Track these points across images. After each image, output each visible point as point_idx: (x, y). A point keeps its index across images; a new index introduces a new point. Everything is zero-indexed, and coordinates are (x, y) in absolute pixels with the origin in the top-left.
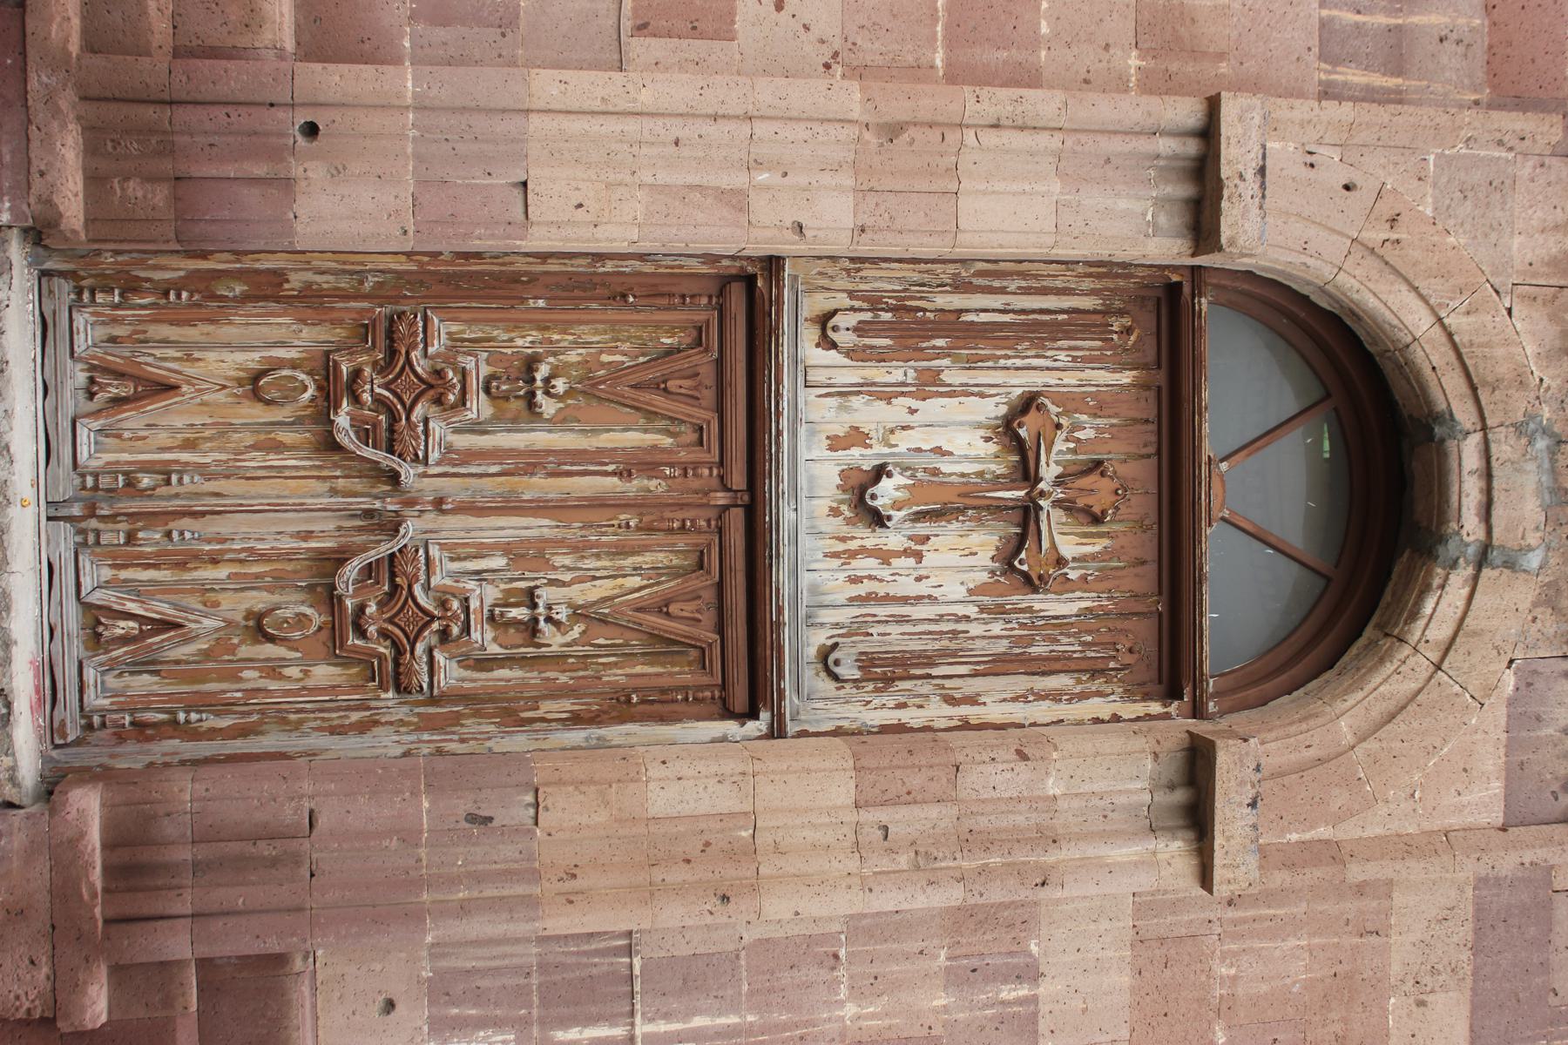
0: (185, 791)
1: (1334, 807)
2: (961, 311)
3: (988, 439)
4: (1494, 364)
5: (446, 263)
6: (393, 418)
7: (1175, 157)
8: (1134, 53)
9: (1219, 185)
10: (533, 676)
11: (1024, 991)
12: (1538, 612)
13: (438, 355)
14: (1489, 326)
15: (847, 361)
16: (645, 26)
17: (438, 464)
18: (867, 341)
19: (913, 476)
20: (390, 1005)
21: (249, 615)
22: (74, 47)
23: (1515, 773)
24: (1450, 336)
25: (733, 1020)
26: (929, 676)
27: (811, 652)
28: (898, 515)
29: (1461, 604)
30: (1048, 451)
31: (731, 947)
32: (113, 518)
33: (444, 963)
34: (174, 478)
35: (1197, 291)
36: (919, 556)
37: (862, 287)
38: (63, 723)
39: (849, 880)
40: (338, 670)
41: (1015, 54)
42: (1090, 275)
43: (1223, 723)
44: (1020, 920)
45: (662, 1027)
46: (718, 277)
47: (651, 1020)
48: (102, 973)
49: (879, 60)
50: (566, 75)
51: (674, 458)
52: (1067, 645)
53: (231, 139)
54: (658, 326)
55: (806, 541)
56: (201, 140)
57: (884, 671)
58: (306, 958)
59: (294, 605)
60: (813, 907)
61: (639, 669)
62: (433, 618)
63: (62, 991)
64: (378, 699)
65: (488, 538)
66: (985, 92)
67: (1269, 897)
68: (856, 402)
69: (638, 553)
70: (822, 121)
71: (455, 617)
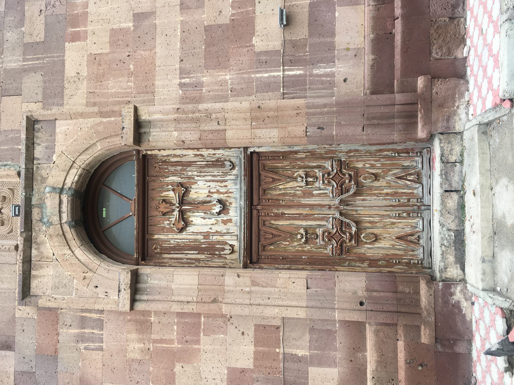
0: (396, 137)
1: (102, 126)
2: (198, 254)
3: (192, 221)
4: (57, 241)
5: (327, 268)
6: (341, 229)
7: (142, 294)
8: (152, 321)
9: (131, 287)
10: (307, 163)
11: (183, 81)
12: (47, 176)
13: (330, 245)
14: (59, 251)
15: (227, 241)
16: (277, 328)
17: (330, 217)
18: (222, 246)
19: (211, 212)
20: (345, 80)
21: (378, 180)
22: (423, 327)
23: (53, 134)
24: (70, 248)
25: (258, 75)
26: (207, 162)
27: (237, 168)
28: (215, 202)
29: (68, 178)
30: (176, 218)
31: (258, 94)
32: (413, 205)
33: (330, 91)
34: (397, 215)
35: (137, 259)
36: (209, 192)
37: (223, 260)
38: (427, 154)
39: (228, 111)
40: (356, 166)
41: (182, 320)
42: (165, 263)
43: (131, 148)
44: (184, 100)
45: (276, 74)
46: (259, 263)
47: (278, 76)
48: (419, 90)
49: (218, 319)
50: (297, 316)
51: (271, 218)
52: (172, 169)
53: (382, 302)
54: (274, 251)
55: (238, 196)
56: (390, 302)
57: (218, 163)
58: (366, 93)
59: (367, 182)
60: (237, 104)
61: (280, 165)
62: (332, 179)
63: (429, 86)
64: (346, 158)
65: (317, 198)
66: (191, 311)
67: (119, 103)
68: (225, 231)
69: (280, 194)
70: (232, 304)
71: (326, 179)
